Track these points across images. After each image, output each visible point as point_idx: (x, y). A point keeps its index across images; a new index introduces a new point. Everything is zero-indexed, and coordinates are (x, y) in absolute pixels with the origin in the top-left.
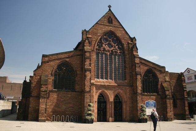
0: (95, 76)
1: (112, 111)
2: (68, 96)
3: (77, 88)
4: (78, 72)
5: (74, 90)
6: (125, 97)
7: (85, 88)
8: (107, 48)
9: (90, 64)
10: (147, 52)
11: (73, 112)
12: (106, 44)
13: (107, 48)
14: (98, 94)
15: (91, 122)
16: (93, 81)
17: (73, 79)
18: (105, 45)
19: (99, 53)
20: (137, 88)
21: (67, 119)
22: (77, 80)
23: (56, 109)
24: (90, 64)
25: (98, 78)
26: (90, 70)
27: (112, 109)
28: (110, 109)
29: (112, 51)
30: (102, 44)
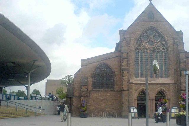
0: (134, 75)
1: (153, 108)
2: (107, 95)
3: (116, 87)
4: (116, 73)
5: (113, 90)
6: (168, 94)
7: (123, 87)
8: (147, 45)
9: (128, 65)
10: (177, 30)
11: (113, 109)
12: (147, 42)
13: (147, 45)
14: (137, 92)
15: (145, 98)
16: (133, 80)
17: (112, 79)
18: (146, 43)
19: (138, 52)
20: (181, 85)
21: (107, 116)
22: (116, 80)
23: (139, 77)
24: (128, 65)
25: (137, 77)
26: (128, 70)
27: (153, 106)
28: (150, 105)
29: (153, 48)
30: (142, 42)
